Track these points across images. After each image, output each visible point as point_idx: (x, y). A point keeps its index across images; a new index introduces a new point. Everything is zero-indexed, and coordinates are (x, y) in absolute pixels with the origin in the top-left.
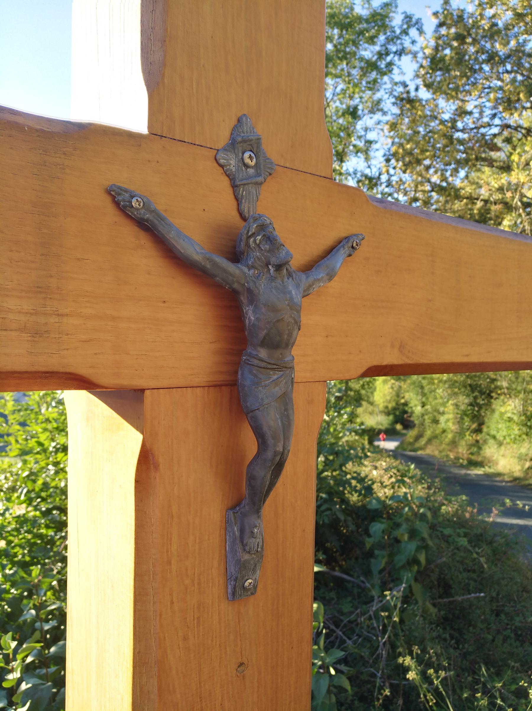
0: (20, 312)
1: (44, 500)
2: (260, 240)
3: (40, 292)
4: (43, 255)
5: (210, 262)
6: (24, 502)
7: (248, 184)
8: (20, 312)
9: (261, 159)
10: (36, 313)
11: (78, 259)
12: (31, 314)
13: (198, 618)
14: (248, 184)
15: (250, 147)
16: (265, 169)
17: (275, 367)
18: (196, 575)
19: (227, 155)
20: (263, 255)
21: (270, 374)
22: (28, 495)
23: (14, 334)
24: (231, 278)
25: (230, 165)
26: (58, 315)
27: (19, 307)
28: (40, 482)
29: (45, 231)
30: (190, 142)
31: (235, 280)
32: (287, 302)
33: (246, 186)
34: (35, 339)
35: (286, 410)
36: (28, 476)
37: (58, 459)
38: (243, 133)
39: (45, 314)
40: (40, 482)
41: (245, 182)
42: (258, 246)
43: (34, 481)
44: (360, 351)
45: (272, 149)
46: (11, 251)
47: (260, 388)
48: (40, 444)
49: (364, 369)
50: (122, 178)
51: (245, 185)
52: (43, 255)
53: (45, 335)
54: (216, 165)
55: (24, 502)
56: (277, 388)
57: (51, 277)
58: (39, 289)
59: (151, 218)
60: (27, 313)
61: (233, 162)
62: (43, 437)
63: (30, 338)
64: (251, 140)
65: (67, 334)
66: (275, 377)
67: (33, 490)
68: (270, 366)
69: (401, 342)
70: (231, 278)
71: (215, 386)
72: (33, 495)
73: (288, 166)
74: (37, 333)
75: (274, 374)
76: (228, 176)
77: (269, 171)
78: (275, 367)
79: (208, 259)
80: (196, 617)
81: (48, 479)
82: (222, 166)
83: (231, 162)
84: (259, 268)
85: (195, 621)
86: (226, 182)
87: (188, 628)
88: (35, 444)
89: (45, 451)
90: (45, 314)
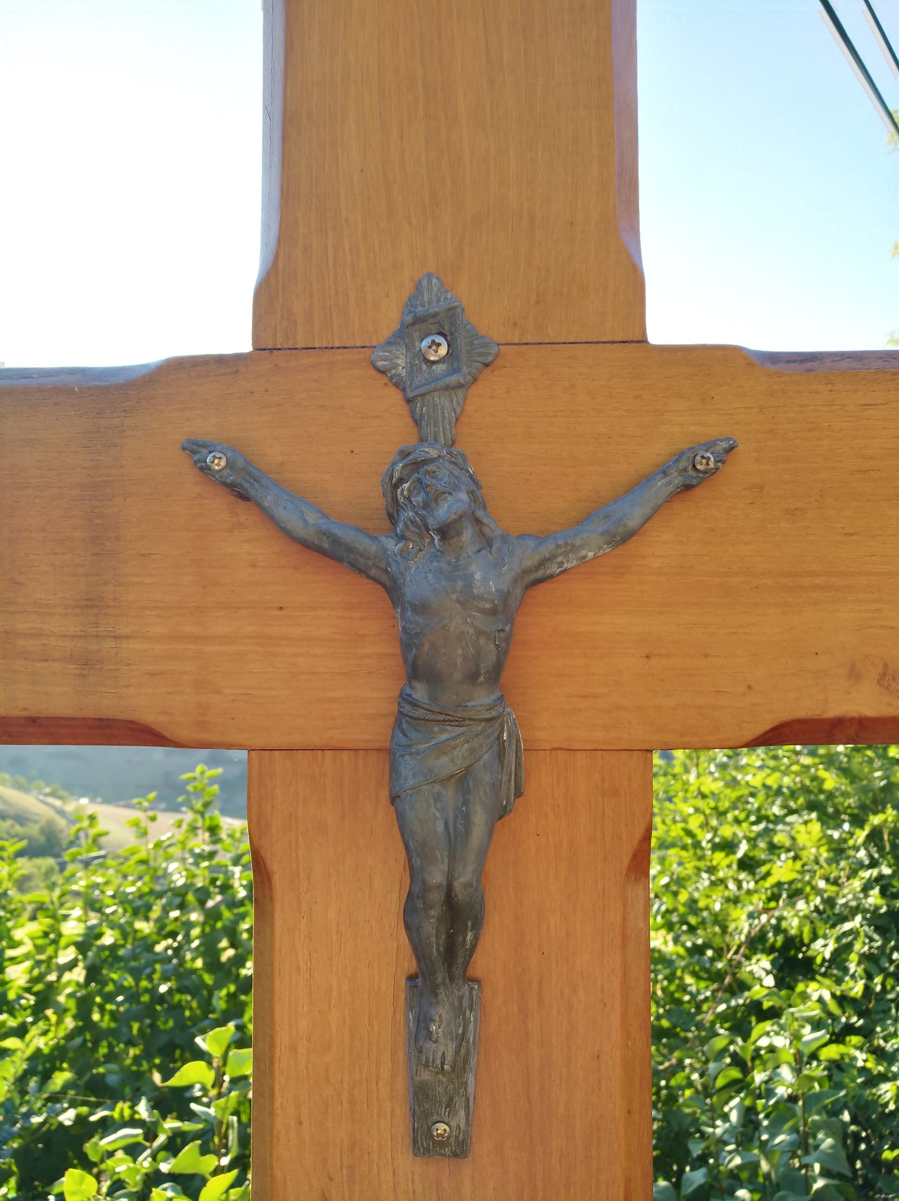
0: (65, 636)
1: (692, 929)
2: (409, 490)
3: (90, 607)
4: (94, 554)
5: (328, 537)
6: (662, 927)
7: (429, 393)
8: (65, 636)
9: (462, 343)
10: (85, 636)
11: (144, 555)
12: (80, 637)
13: (351, 1168)
14: (429, 393)
15: (434, 328)
16: (474, 358)
17: (442, 717)
18: (345, 1085)
19: (391, 352)
20: (417, 513)
21: (433, 732)
22: (668, 916)
23: (56, 665)
24: (362, 561)
25: (396, 366)
26: (115, 637)
27: (63, 629)
28: (683, 897)
29: (98, 521)
30: (324, 345)
31: (370, 563)
32: (454, 597)
33: (428, 397)
34: (85, 672)
35: (465, 802)
36: (667, 886)
37: (715, 863)
38: (423, 305)
39: (97, 636)
40: (683, 897)
41: (423, 390)
42: (409, 499)
43: (675, 894)
44: (749, 687)
45: (488, 318)
46: (55, 554)
47: (407, 758)
48: (689, 833)
49: (767, 727)
50: (204, 426)
51: (423, 395)
52: (94, 554)
53: (97, 667)
54: (373, 372)
55: (662, 927)
56: (444, 760)
57: (106, 583)
58: (89, 603)
59: (239, 480)
60: (73, 636)
61: (401, 362)
62: (694, 824)
63: (77, 671)
64: (435, 315)
65: (128, 665)
66: (444, 736)
67: (675, 910)
68: (432, 717)
69: (886, 666)
70: (362, 561)
71: (379, 750)
72: (675, 918)
73: (529, 341)
74: (87, 663)
75: (442, 731)
76: (396, 385)
77: (481, 359)
78: (442, 717)
79: (324, 534)
80: (345, 1164)
81: (696, 895)
82: (383, 372)
83: (399, 361)
84: (414, 538)
85: (345, 1172)
86: (394, 397)
87: (331, 1179)
88: (682, 833)
89: (697, 845)
90: (97, 636)
